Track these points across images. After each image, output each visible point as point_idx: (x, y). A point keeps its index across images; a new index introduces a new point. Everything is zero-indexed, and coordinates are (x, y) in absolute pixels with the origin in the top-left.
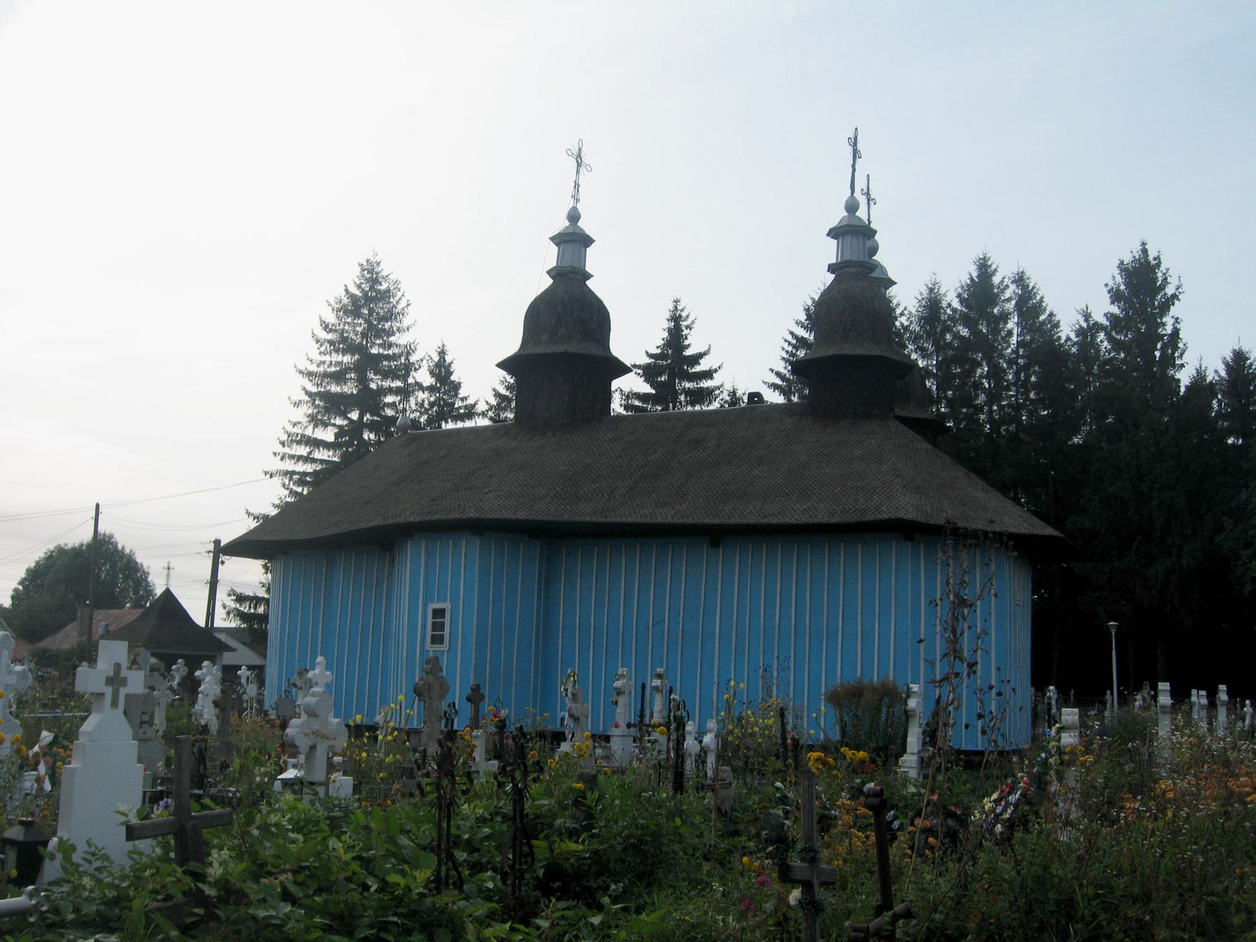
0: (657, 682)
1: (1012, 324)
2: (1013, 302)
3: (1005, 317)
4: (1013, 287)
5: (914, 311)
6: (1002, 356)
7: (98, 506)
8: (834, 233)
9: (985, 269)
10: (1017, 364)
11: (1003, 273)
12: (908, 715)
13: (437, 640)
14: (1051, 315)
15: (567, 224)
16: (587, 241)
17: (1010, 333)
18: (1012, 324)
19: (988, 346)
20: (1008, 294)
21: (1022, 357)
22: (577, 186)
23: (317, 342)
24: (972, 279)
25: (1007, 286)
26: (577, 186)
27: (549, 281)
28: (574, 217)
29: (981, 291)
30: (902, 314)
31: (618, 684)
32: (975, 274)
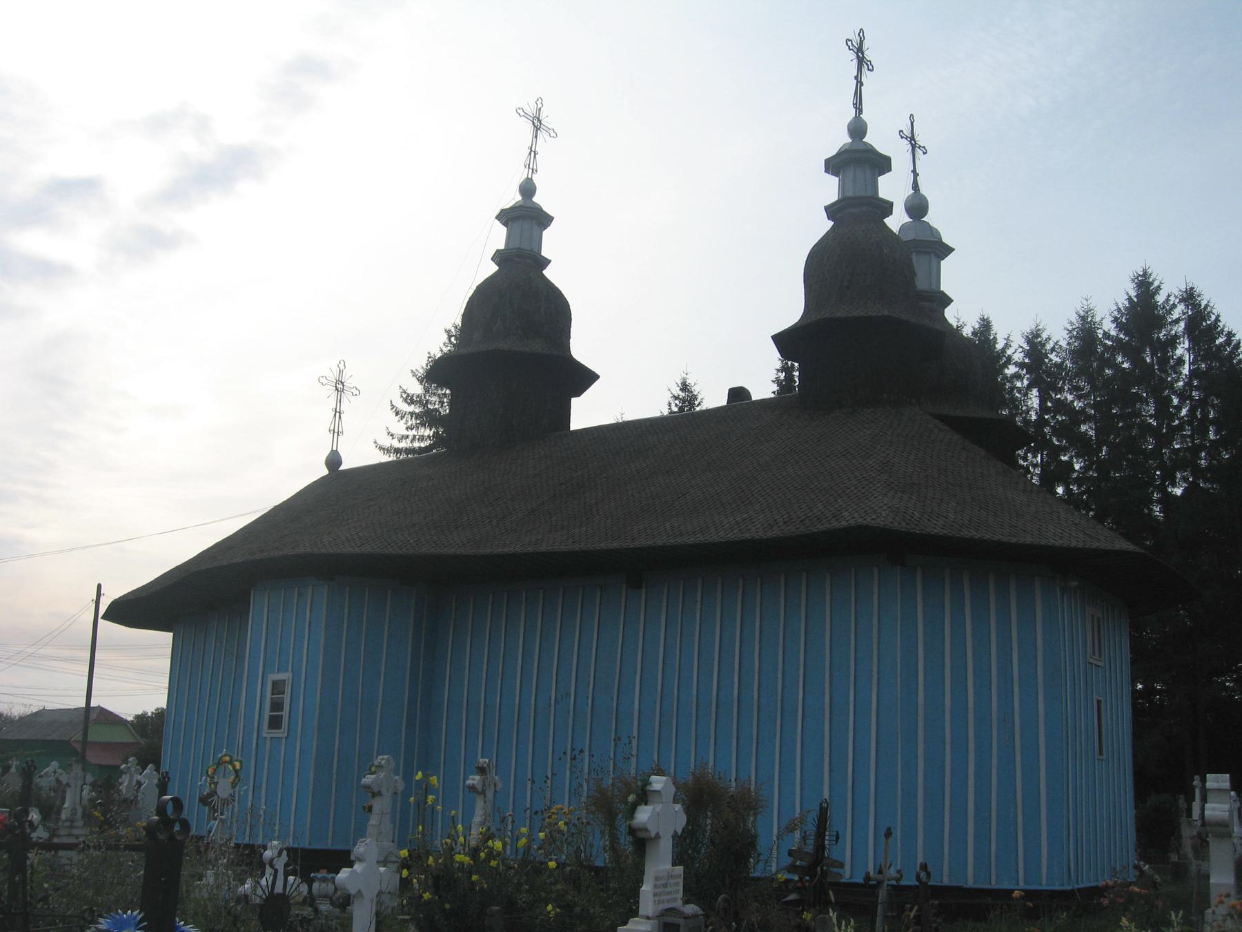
0: (474, 780)
1: (1182, 349)
2: (1182, 324)
3: (1173, 342)
4: (1181, 307)
5: (1064, 344)
6: (1171, 386)
7: (99, 586)
8: (834, 165)
9: (1145, 286)
10: (1191, 398)
11: (1169, 288)
12: (642, 842)
13: (275, 723)
14: (1230, 335)
15: (519, 198)
16: (543, 220)
17: (1180, 361)
18: (1182, 349)
19: (1154, 379)
20: (1176, 314)
21: (1197, 388)
22: (533, 152)
23: (397, 414)
24: (1130, 299)
25: (1174, 306)
26: (533, 152)
27: (494, 268)
28: (528, 189)
29: (1143, 311)
30: (1053, 350)
31: (368, 779)
32: (1133, 293)
